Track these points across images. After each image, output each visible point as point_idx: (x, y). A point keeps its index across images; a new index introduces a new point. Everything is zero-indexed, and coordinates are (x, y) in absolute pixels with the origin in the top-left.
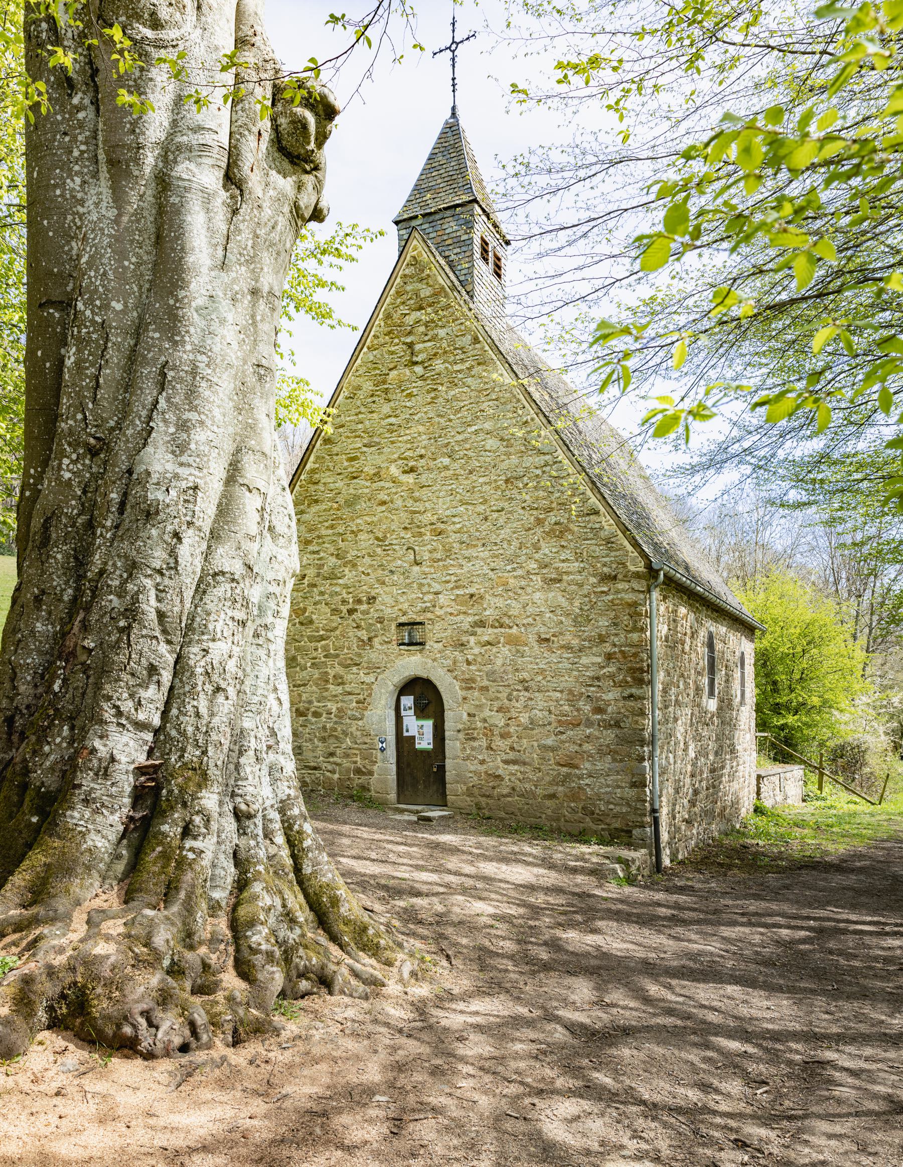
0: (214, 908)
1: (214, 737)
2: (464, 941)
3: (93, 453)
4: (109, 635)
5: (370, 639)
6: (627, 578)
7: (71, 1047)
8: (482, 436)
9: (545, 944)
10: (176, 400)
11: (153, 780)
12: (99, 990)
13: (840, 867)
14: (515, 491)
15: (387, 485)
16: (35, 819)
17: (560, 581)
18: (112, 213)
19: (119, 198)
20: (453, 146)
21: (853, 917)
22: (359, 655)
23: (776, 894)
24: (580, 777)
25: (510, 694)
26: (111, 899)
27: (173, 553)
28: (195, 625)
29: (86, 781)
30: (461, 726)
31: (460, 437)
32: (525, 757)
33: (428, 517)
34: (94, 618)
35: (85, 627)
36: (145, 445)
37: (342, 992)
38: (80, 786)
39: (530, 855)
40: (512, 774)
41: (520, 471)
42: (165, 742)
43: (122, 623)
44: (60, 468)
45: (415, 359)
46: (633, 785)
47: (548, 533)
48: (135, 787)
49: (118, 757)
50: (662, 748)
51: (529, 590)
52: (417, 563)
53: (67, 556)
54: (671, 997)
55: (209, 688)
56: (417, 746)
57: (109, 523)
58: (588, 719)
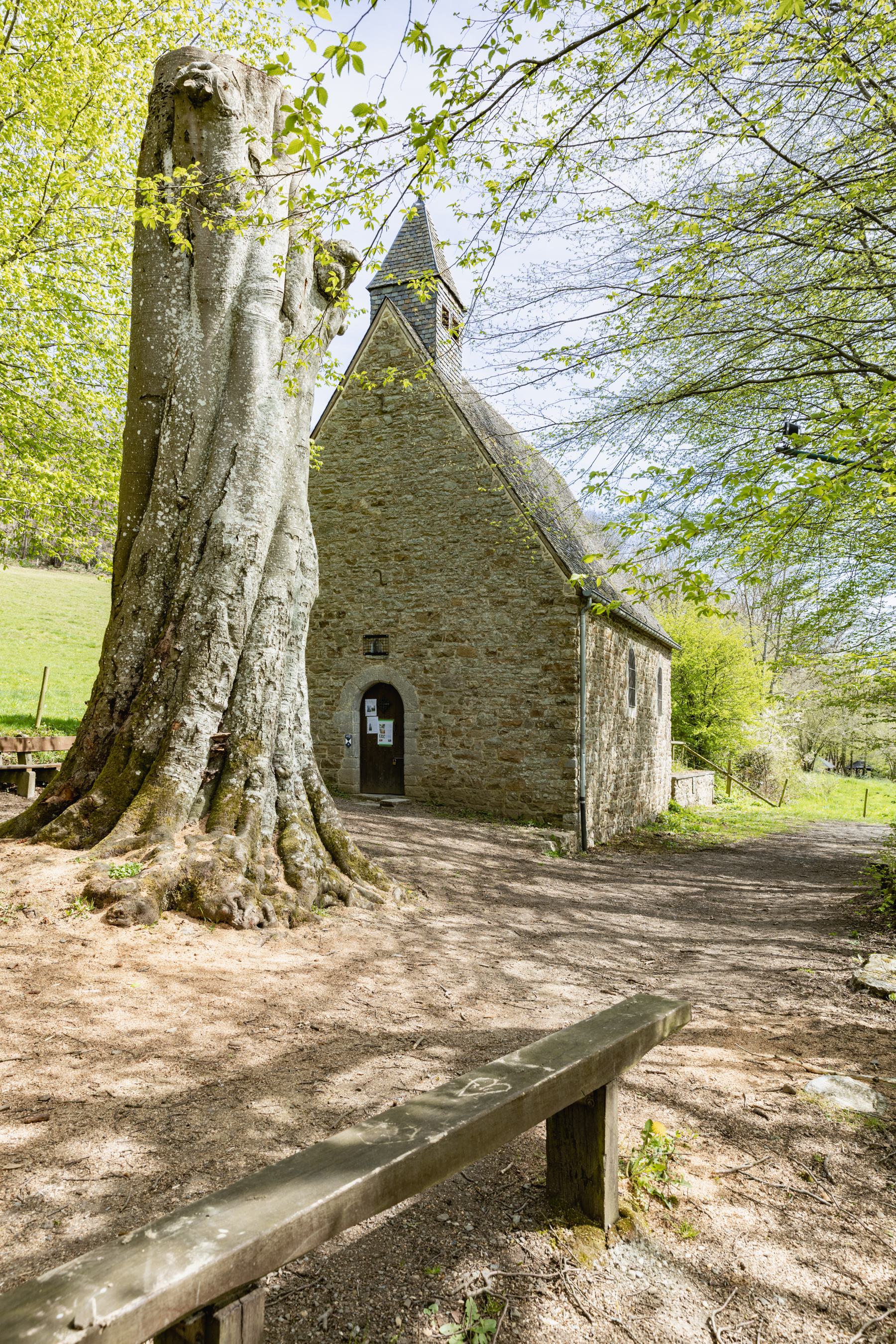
0: (265, 840)
1: (266, 716)
2: (434, 884)
3: (181, 508)
4: (194, 641)
5: (339, 649)
6: (562, 603)
7: (186, 921)
8: (441, 478)
9: (496, 888)
10: (243, 472)
11: (223, 746)
12: (204, 884)
13: (737, 851)
14: (469, 526)
15: (358, 515)
16: (138, 773)
17: (505, 603)
18: (200, 336)
19: (205, 325)
20: (420, 227)
21: (738, 881)
22: (329, 663)
23: (679, 867)
24: (520, 770)
25: (461, 699)
26: (196, 828)
27: (240, 583)
28: (253, 635)
29: (178, 745)
30: (418, 726)
31: (422, 478)
32: (473, 753)
33: (393, 545)
34: (183, 628)
35: (176, 634)
36: (220, 504)
37: (355, 905)
38: (174, 749)
39: (478, 833)
40: (461, 767)
41: (474, 509)
42: (231, 720)
43: (204, 633)
44: (155, 518)
45: (384, 409)
46: (564, 777)
47: (496, 563)
48: (211, 751)
49: (200, 729)
50: (589, 746)
51: (480, 610)
52: (383, 584)
53: (158, 582)
54: (590, 918)
55: (263, 681)
56: (379, 743)
57: (191, 560)
58: (527, 721)
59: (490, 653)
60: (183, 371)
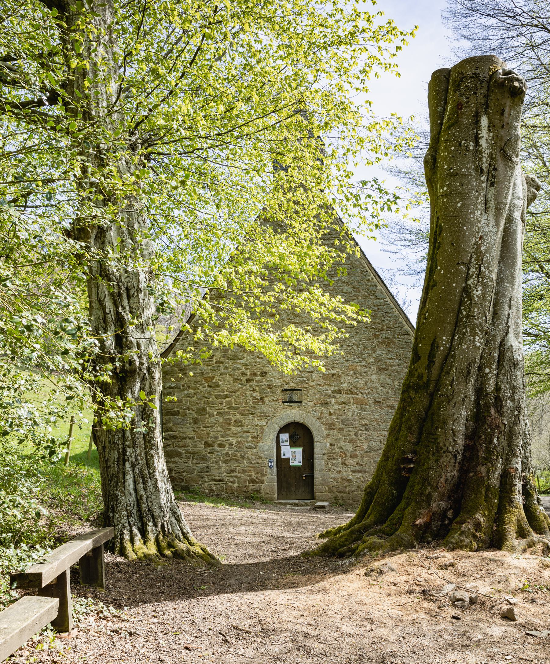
17: (387, 369)
25: (357, 432)
30: (326, 452)
32: (366, 468)
43: (516, 413)
44: (474, 341)
47: (381, 343)
56: (291, 464)
59: (376, 402)
60: (487, 250)
